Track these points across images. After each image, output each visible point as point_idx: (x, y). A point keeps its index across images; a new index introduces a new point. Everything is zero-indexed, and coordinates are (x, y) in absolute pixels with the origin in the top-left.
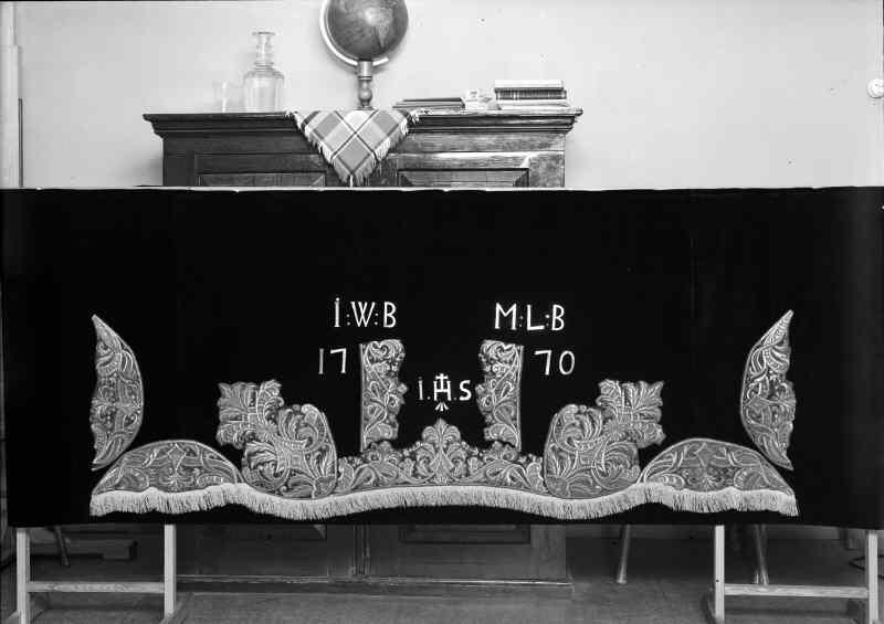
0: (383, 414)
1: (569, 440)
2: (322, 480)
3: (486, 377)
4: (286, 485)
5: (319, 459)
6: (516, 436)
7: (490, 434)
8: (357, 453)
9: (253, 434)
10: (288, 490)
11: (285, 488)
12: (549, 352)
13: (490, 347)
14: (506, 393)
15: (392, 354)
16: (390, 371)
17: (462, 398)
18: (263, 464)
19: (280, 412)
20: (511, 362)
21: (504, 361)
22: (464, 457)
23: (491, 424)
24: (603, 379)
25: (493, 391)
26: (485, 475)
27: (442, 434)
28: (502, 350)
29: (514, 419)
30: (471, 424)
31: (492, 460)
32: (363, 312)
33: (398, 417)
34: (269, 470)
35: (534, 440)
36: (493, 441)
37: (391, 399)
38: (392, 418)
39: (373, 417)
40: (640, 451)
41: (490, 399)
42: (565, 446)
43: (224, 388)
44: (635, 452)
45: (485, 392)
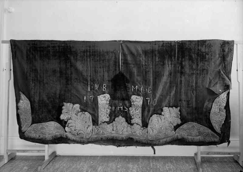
0: (105, 115)
1: (75, 130)
2: (87, 134)
3: (132, 105)
4: (77, 133)
5: (87, 128)
6: (140, 122)
7: (133, 121)
8: (98, 125)
9: (70, 118)
10: (78, 135)
11: (77, 134)
12: (149, 98)
13: (134, 97)
14: (138, 110)
15: (107, 98)
16: (107, 103)
17: (125, 110)
18: (72, 126)
19: (79, 113)
20: (139, 102)
21: (137, 101)
22: (126, 127)
23: (133, 119)
24: (60, 119)
25: (134, 109)
26: (132, 132)
27: (121, 120)
28: (137, 98)
29: (140, 117)
30: (129, 120)
31: (134, 128)
32: (96, 87)
33: (109, 115)
34: (73, 129)
35: (145, 125)
36: (134, 124)
37: (107, 110)
38: (108, 116)
39: (102, 116)
40: (174, 127)
41: (133, 111)
42: (76, 132)
43: (65, 104)
44: (173, 127)
45: (132, 110)
